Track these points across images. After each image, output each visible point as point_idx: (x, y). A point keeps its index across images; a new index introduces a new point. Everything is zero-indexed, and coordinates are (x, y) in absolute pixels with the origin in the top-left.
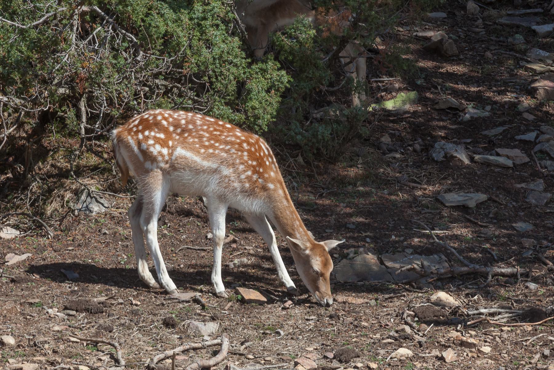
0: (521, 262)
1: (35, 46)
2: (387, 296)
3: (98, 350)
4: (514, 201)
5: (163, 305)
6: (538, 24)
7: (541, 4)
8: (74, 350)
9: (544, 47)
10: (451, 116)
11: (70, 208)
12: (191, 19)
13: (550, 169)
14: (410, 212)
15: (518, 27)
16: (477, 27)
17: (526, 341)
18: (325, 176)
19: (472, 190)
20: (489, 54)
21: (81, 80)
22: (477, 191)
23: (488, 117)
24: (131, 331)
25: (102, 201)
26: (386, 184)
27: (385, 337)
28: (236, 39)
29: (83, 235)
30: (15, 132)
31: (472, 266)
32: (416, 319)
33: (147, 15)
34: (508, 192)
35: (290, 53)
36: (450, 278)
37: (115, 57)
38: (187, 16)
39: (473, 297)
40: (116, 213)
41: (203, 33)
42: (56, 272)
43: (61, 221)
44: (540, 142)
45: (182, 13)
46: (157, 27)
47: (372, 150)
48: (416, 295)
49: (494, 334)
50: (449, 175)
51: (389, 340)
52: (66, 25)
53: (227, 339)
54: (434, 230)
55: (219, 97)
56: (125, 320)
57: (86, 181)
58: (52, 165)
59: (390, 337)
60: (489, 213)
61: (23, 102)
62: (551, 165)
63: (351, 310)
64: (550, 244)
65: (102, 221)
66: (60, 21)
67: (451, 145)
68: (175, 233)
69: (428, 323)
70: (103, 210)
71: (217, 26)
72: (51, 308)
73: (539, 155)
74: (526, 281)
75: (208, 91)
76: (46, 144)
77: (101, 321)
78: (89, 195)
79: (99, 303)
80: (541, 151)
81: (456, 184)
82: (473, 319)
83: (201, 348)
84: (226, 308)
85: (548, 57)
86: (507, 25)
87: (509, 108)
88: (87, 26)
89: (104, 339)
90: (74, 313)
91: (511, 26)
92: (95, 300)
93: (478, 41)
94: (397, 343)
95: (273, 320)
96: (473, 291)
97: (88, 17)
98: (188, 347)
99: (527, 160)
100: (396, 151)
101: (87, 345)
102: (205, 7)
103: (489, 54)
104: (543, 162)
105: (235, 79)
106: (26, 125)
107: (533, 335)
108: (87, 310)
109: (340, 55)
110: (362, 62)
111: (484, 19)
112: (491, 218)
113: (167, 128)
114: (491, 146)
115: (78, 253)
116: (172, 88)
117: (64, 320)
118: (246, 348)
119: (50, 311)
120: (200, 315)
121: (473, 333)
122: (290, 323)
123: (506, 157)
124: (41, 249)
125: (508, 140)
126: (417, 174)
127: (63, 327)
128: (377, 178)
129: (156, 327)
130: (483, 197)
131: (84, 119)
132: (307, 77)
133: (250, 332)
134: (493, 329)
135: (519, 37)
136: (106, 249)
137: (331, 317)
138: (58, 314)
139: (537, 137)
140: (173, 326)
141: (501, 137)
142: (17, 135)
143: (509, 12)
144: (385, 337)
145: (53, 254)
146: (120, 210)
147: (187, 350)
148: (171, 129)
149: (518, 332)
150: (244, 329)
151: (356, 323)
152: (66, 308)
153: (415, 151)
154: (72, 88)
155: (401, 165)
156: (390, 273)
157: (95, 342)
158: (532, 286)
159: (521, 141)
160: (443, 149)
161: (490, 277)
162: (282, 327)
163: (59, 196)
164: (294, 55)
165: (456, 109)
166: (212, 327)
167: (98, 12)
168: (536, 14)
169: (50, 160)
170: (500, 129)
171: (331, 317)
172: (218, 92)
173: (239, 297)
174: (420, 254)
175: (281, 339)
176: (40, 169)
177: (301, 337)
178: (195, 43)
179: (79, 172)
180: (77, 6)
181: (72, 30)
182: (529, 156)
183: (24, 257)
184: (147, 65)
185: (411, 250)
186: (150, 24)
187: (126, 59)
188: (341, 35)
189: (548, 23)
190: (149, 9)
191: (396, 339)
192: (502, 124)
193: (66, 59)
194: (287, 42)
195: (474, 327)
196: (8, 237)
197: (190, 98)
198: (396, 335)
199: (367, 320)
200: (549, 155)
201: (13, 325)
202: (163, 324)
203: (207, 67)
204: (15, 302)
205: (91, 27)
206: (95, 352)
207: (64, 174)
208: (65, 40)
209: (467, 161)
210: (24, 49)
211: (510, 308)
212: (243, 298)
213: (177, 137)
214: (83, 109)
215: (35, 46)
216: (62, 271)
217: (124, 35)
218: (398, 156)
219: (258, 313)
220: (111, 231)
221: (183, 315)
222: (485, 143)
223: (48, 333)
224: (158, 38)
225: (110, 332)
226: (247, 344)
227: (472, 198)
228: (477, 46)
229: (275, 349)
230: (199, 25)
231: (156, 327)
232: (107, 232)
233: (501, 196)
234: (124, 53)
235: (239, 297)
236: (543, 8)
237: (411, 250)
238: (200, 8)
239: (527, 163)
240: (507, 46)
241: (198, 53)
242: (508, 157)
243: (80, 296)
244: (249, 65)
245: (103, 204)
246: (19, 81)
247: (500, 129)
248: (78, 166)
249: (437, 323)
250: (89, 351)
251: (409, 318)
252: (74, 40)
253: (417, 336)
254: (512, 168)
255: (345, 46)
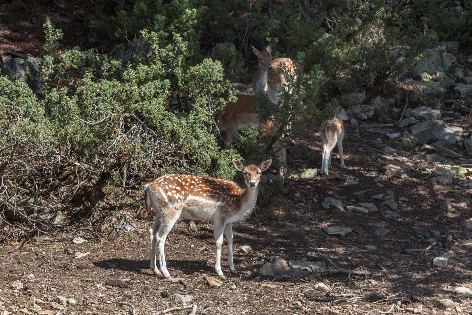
0: (370, 268)
1: (98, 135)
2: (290, 284)
3: (122, 309)
4: (367, 233)
5: (162, 284)
6: (390, 133)
7: (393, 121)
8: (109, 308)
9: (392, 146)
10: (336, 183)
11: (114, 227)
12: (188, 123)
13: (390, 215)
14: (307, 237)
15: (379, 134)
16: (356, 133)
17: (366, 312)
18: (261, 215)
19: (344, 226)
20: (361, 149)
21: (123, 155)
22: (347, 226)
23: (357, 185)
24: (142, 299)
25: (133, 224)
26: (295, 221)
27: (286, 307)
28: (213, 135)
29: (120, 243)
30: (87, 183)
31: (340, 269)
32: (305, 298)
33: (162, 120)
34: (364, 228)
35: (244, 144)
36: (326, 275)
37: (143, 143)
38: (185, 121)
39: (339, 286)
40: (140, 231)
41: (194, 131)
42: (104, 264)
43: (109, 234)
44: (385, 200)
45: (183, 119)
46: (167, 126)
47: (289, 201)
48: (306, 284)
49: (348, 308)
50: (331, 217)
51: (289, 310)
52: (116, 123)
53: (196, 305)
54: (320, 247)
55: (201, 167)
56: (140, 292)
57: (124, 213)
58: (106, 203)
59: (289, 308)
60: (353, 239)
61: (89, 166)
62: (390, 213)
63: (268, 291)
64: (385, 258)
65: (132, 235)
66: (113, 121)
67: (334, 200)
68: (173, 244)
69: (312, 300)
70: (133, 229)
71: (202, 127)
72: (98, 284)
73: (384, 207)
74: (370, 279)
75: (195, 164)
76: (104, 191)
77: (126, 292)
78: (125, 220)
79: (126, 282)
80: (385, 205)
81: (335, 222)
82: (337, 299)
83: (181, 310)
84: (198, 288)
85: (394, 152)
86: (373, 133)
87: (370, 180)
88: (129, 125)
89: (126, 303)
90: (111, 287)
91: (375, 134)
92: (124, 280)
93: (355, 142)
94: (293, 311)
95: (224, 295)
96: (340, 283)
97: (129, 120)
98: (173, 309)
99: (377, 210)
100: (303, 202)
101: (117, 305)
102: (196, 117)
103: (361, 149)
104: (386, 212)
105: (211, 157)
106: (93, 179)
107: (371, 309)
108: (118, 286)
109: (273, 146)
110: (284, 151)
111: (360, 129)
112: (353, 242)
113: (182, 183)
114: (357, 201)
115: (117, 253)
116: (176, 161)
117: (105, 291)
118: (207, 311)
119: (98, 285)
120: (182, 291)
121: (337, 307)
122: (233, 297)
123: (365, 208)
124: (95, 250)
125: (367, 199)
126: (313, 215)
127: (103, 295)
128: (290, 217)
129: (157, 297)
130: (349, 230)
131: (125, 177)
132: (252, 158)
133: (210, 302)
134: (348, 305)
135: (379, 140)
136: (133, 251)
137: (257, 295)
138: (102, 287)
139: (383, 197)
140: (167, 297)
141: (363, 196)
142: (88, 185)
143: (374, 126)
144: (286, 307)
145: (102, 253)
146: (143, 230)
147: (173, 311)
148: (184, 183)
149: (362, 307)
150: (207, 300)
151: (271, 299)
152: (107, 284)
153: (313, 202)
154: (118, 160)
155: (304, 210)
156: (293, 271)
157: (121, 304)
158: (373, 282)
159: (374, 199)
160: (329, 202)
161: (349, 276)
162: (228, 299)
163: (108, 221)
164: (246, 146)
165: (339, 179)
166: (189, 298)
167: (134, 117)
168: (390, 127)
169: (105, 200)
170: (363, 192)
171: (257, 295)
172: (201, 165)
173: (206, 282)
174: (311, 261)
175: (227, 306)
176: (99, 204)
177: (238, 306)
178: (189, 136)
179: (121, 207)
180: (122, 113)
181: (119, 127)
182: (378, 207)
183: (86, 254)
184: (160, 148)
185: (306, 259)
186: (163, 125)
187: (150, 144)
188: (273, 135)
189: (396, 133)
190: (164, 117)
191: (292, 309)
192: (364, 189)
193: (114, 143)
194: (242, 138)
195: (337, 304)
196: (78, 242)
197: (185, 167)
198: (293, 306)
199: (277, 298)
200: (390, 207)
201: (76, 293)
202: (161, 295)
203: (195, 151)
204: (78, 279)
205: (131, 125)
206: (121, 310)
207: (112, 208)
208: (115, 132)
209: (342, 210)
210: (91, 136)
211: (359, 294)
212: (208, 282)
213: (187, 188)
214: (125, 171)
215: (98, 135)
216: (107, 263)
217: (149, 131)
218: (303, 205)
219: (216, 291)
220: (136, 241)
221: (173, 290)
222: (354, 199)
223: (95, 298)
224: (168, 133)
225: (130, 299)
226: (208, 309)
227: (343, 231)
228: (355, 144)
229: (223, 312)
230: (192, 126)
231: (157, 297)
232: (134, 242)
233: (360, 230)
234: (149, 141)
235: (206, 282)
236: (394, 124)
237: (306, 259)
238: (193, 117)
239: (377, 212)
240: (372, 145)
241: (190, 142)
242: (366, 208)
243: (116, 278)
244: (219, 150)
245: (133, 226)
246: (87, 155)
247: (363, 192)
248: (121, 204)
249: (317, 301)
250: (117, 309)
251: (301, 297)
252: (120, 132)
253: (304, 308)
254: (368, 214)
255: (275, 142)
